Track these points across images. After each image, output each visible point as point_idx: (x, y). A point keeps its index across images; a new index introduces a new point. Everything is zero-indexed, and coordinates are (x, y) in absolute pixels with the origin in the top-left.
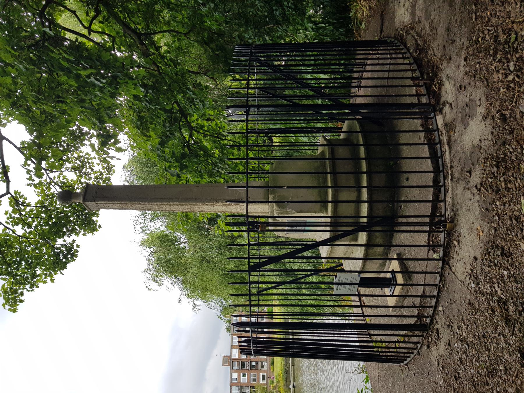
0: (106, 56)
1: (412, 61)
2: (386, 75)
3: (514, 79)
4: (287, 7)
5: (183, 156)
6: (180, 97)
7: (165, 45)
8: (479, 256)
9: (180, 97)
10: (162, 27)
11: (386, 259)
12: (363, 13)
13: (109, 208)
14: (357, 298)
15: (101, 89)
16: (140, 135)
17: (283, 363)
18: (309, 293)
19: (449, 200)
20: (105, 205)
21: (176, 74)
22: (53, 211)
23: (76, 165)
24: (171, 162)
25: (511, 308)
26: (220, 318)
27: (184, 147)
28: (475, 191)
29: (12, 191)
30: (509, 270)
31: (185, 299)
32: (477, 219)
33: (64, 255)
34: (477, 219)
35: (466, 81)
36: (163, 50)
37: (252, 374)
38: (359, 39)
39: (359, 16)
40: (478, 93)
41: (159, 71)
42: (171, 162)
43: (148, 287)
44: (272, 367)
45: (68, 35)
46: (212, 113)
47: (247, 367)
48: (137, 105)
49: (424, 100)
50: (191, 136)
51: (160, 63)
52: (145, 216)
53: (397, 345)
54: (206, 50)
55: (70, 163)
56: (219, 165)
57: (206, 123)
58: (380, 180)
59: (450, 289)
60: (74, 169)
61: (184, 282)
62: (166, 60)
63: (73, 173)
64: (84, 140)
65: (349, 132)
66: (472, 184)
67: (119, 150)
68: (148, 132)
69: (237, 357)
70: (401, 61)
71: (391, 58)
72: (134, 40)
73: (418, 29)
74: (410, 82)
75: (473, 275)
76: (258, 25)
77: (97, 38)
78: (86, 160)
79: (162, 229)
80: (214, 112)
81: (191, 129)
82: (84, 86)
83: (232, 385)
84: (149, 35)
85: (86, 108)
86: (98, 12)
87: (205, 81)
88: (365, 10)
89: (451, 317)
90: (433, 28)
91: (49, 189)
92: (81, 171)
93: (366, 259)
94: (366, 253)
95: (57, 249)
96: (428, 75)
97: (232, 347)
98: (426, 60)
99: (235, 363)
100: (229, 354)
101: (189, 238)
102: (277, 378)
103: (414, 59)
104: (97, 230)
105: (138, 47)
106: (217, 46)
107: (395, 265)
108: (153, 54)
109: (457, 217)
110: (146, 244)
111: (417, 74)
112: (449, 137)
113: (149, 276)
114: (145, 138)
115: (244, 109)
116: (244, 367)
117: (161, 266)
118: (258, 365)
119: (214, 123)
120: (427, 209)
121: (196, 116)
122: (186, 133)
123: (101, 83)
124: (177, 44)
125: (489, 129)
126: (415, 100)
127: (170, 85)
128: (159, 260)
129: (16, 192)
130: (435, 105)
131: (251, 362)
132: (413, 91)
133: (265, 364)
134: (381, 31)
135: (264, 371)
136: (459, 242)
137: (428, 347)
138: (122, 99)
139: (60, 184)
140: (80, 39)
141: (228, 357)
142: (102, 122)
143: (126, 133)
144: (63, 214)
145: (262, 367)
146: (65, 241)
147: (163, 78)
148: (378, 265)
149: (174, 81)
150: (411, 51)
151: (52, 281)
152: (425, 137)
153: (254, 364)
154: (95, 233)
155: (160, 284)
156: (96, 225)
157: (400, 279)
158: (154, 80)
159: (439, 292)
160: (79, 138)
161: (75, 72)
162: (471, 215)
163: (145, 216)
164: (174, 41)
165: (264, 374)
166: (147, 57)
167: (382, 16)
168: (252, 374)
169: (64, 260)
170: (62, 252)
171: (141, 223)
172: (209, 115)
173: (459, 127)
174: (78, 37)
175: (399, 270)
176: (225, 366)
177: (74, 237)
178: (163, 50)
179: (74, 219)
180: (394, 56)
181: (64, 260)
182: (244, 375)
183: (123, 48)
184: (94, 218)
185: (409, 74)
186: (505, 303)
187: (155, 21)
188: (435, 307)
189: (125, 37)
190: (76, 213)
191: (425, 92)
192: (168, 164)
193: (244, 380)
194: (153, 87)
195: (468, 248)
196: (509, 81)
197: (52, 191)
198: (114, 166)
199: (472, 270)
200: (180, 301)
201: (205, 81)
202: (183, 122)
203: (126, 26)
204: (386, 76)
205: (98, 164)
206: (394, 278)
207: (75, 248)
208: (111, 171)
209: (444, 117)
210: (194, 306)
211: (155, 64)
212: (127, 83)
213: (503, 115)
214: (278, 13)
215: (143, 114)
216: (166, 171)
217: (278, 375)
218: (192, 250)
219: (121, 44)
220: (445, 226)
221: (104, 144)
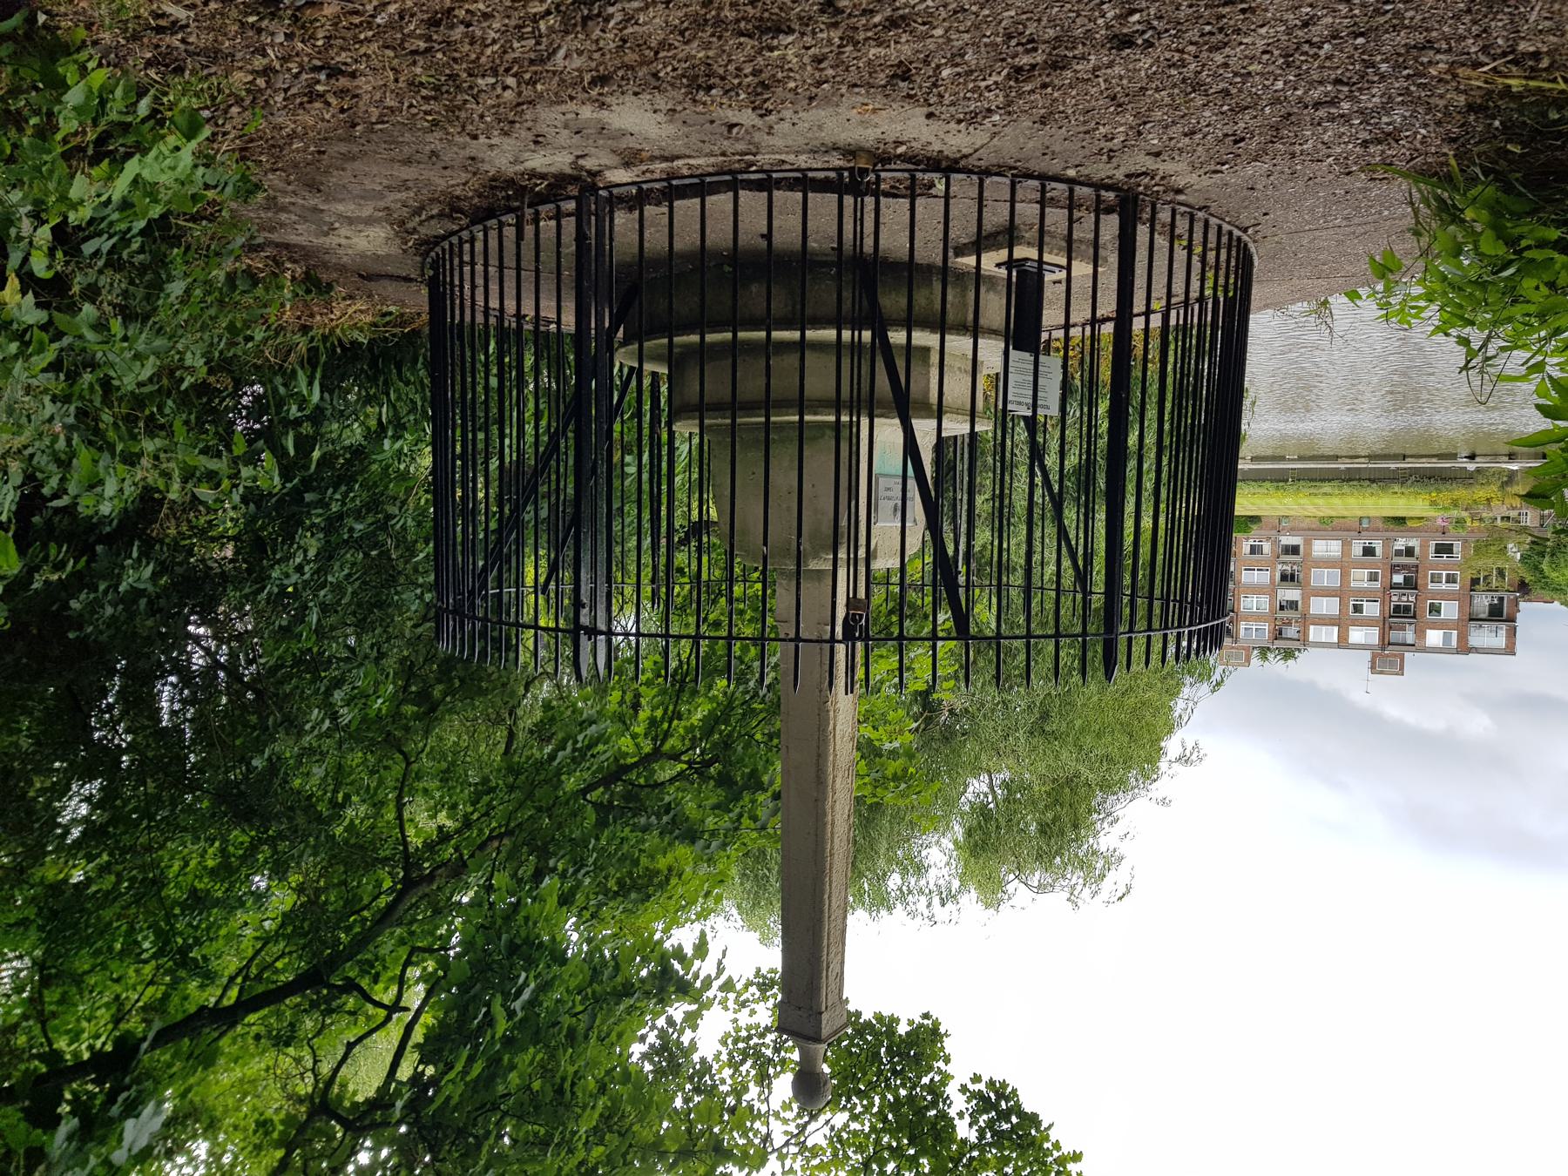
0: (462, 970)
2: (510, 275)
3: (514, 75)
4: (344, 504)
5: (724, 780)
6: (571, 783)
7: (434, 816)
8: (926, 110)
9: (571, 783)
10: (388, 822)
12: (361, 311)
13: (840, 976)
15: (544, 987)
16: (666, 895)
17: (1397, 488)
18: (1137, 426)
19: (803, 161)
20: (833, 986)
21: (511, 788)
22: (878, 1141)
23: (753, 1072)
24: (740, 816)
25: (1025, 60)
26: (1218, 684)
27: (704, 778)
28: (772, 118)
30: (938, 66)
31: (1160, 788)
32: (838, 114)
33: (999, 1119)
34: (838, 114)
36: (449, 823)
37: (1430, 586)
38: (425, 317)
39: (369, 319)
40: (549, 117)
41: (500, 837)
42: (740, 816)
43: (1119, 894)
44: (1409, 524)
45: (404, 1073)
46: (616, 696)
47: (1409, 598)
48: (588, 898)
49: (571, 206)
50: (675, 757)
51: (481, 831)
52: (910, 892)
53: (1198, 250)
54: (451, 711)
55: (746, 1090)
56: (752, 684)
57: (644, 715)
58: (754, 296)
59: (1017, 155)
60: (764, 1079)
61: (1107, 787)
62: (475, 816)
63: (775, 1082)
64: (679, 1043)
66: (759, 122)
67: (701, 949)
68: (658, 872)
70: (479, 246)
71: (473, 263)
72: (421, 898)
73: (405, 212)
75: (972, 119)
76: (382, 577)
77: (415, 996)
78: (741, 1045)
79: (951, 846)
80: (613, 689)
81: (656, 754)
82: (531, 1030)
83: (1464, 648)
84: (409, 860)
85: (591, 1028)
86: (351, 986)
87: (530, 713)
88: (354, 308)
89: (1087, 152)
90: (404, 185)
91: (815, 1151)
92: (770, 1060)
93: (976, 331)
94: (961, 329)
95: (981, 1136)
96: (511, 198)
97: (1343, 643)
98: (476, 200)
99: (1395, 635)
100: (1367, 655)
101: (976, 771)
102: (1445, 508)
103: (473, 223)
104: (936, 1024)
105: (439, 888)
106: (439, 681)
107: (991, 261)
108: (457, 849)
109: (841, 144)
110: (992, 894)
112: (653, 158)
113: (1087, 891)
114: (674, 881)
115: (583, 638)
116: (1407, 609)
117: (1059, 853)
118: (1404, 567)
119: (643, 689)
121: (626, 743)
122: (666, 771)
123: (526, 984)
124: (433, 784)
125: (629, 98)
126: (569, 224)
127: (539, 809)
128: (1039, 857)
130: (582, 187)
132: (548, 226)
133: (1400, 544)
134: (407, 279)
135: (1424, 546)
137: (1179, 191)
138: (572, 935)
139: (806, 1119)
140: (418, 1036)
142: (627, 990)
143: (666, 931)
144: (890, 1116)
145: (1409, 552)
146: (961, 1115)
147: (520, 824)
148: (991, 295)
149: (530, 796)
150: (456, 228)
151: (1076, 1157)
152: (658, 204)
153: (1398, 578)
154: (942, 1031)
155: (1113, 860)
156: (921, 1026)
158: (525, 849)
159: (1029, 176)
160: (671, 1055)
161: (498, 1046)
162: (830, 124)
163: (910, 892)
164: (426, 791)
165: (1432, 549)
166: (465, 865)
167: (370, 277)
168: (1430, 586)
169: (1014, 1120)
170: (990, 1124)
171: (929, 905)
172: (621, 703)
173: (632, 143)
174: (410, 1043)
176: (1402, 668)
177: (952, 1090)
178: (449, 823)
179: (903, 1085)
180: (467, 258)
181: (1014, 1120)
182: (1435, 609)
183: (442, 931)
184: (902, 1029)
185: (510, 232)
187: (372, 842)
188: (1071, 182)
189: (411, 923)
190: (887, 1080)
191: (552, 206)
192: (746, 821)
193: (1450, 610)
194: (544, 853)
195: (908, 126)
196: (519, 84)
197: (824, 1143)
198: (759, 970)
199: (959, 122)
200: (1164, 802)
201: (530, 713)
202: (638, 776)
203: (386, 917)
204: (513, 273)
205: (753, 1012)
207: (982, 1086)
208: (772, 979)
209: (609, 168)
210: (1184, 759)
211: (482, 847)
212: (527, 919)
213: (593, 82)
214: (359, 527)
215: (612, 884)
216: (764, 828)
217: (1433, 503)
218: (1011, 762)
219: (432, 933)
221: (684, 989)
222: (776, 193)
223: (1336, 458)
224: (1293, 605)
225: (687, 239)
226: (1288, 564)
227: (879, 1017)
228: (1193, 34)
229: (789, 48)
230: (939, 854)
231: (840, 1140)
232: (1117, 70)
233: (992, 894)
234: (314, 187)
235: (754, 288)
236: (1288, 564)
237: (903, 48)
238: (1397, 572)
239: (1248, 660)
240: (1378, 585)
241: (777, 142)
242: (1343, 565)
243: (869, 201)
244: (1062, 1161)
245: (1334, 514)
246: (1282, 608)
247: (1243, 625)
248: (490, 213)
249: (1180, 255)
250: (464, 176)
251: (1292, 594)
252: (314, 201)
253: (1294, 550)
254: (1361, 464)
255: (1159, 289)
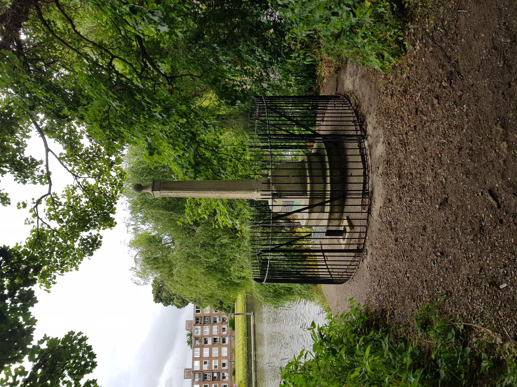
1: (353, 112)
8: (382, 206)
11: (341, 219)
14: (323, 257)
17: (245, 370)
19: (370, 182)
25: (393, 223)
28: (380, 176)
29: (51, 193)
35: (376, 126)
40: (381, 132)
44: (233, 377)
65: (319, 149)
66: (379, 173)
69: (198, 369)
71: (342, 107)
74: (351, 123)
75: (380, 216)
93: (329, 219)
96: (361, 120)
97: (194, 359)
99: (197, 375)
100: (190, 367)
103: (354, 110)
104: (114, 226)
107: (345, 223)
110: (133, 244)
111: (356, 119)
112: (370, 151)
116: (206, 378)
120: (361, 187)
125: (385, 148)
129: (54, 194)
130: (364, 136)
131: (213, 374)
133: (226, 374)
134: (337, 90)
135: (226, 382)
136: (374, 202)
137: (363, 261)
141: (190, 369)
145: (224, 377)
146: (91, 233)
151: (77, 269)
152: (360, 152)
153: (215, 375)
157: (348, 229)
159: (367, 229)
162: (379, 188)
165: (225, 384)
170: (89, 242)
173: (374, 147)
175: (347, 225)
176: (186, 378)
184: (111, 215)
185: (352, 119)
186: (391, 223)
188: (365, 238)
206: (345, 229)
207: (99, 239)
213: (388, 142)
217: (241, 382)
220: (368, 195)
222: (363, 177)
223: (255, 350)
224: (206, 342)
225: (351, 159)
226: (219, 340)
227: (115, 209)
228: (398, 252)
229: (395, 180)
230: (147, 228)
231: (77, 199)
232: (391, 241)
233: (133, 244)
234: (363, 76)
235: (339, 172)
236: (219, 340)
237: (395, 200)
238: (217, 374)
239: (188, 330)
240: (213, 368)
241: (374, 177)
242: (220, 357)
243: (361, 196)
244: (75, 265)
245: (236, 352)
246: (205, 339)
247: (199, 327)
248: (357, 114)
249: (349, 263)
250: (366, 110)
251: (210, 342)
252: (359, 75)
253: (224, 342)
254: (253, 358)
255: (326, 273)
